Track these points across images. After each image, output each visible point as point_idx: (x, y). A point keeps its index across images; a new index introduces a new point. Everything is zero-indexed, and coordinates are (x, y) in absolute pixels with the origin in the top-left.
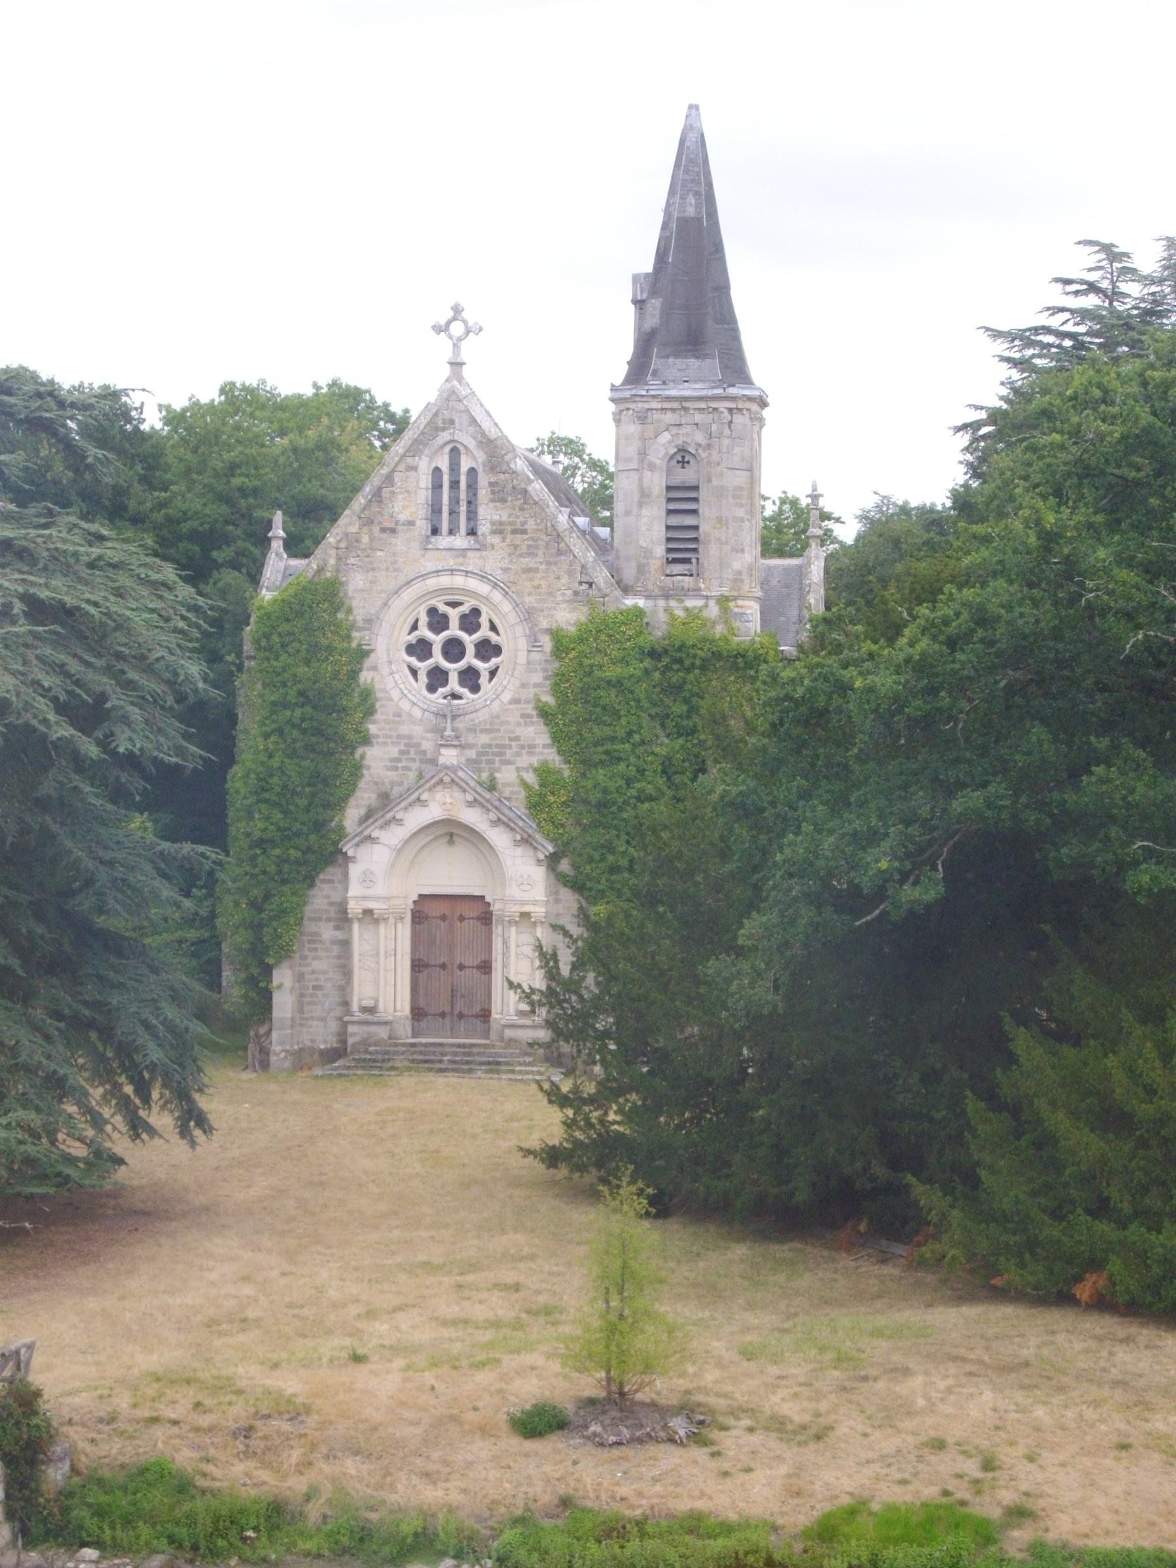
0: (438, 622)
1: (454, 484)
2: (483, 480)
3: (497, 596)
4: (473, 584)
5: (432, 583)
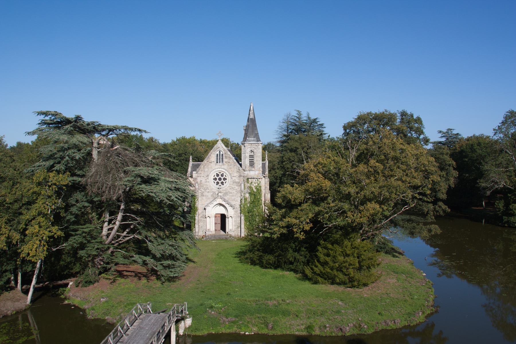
0: (218, 175)
1: (220, 156)
2: (224, 155)
3: (226, 172)
4: (223, 170)
5: (217, 170)
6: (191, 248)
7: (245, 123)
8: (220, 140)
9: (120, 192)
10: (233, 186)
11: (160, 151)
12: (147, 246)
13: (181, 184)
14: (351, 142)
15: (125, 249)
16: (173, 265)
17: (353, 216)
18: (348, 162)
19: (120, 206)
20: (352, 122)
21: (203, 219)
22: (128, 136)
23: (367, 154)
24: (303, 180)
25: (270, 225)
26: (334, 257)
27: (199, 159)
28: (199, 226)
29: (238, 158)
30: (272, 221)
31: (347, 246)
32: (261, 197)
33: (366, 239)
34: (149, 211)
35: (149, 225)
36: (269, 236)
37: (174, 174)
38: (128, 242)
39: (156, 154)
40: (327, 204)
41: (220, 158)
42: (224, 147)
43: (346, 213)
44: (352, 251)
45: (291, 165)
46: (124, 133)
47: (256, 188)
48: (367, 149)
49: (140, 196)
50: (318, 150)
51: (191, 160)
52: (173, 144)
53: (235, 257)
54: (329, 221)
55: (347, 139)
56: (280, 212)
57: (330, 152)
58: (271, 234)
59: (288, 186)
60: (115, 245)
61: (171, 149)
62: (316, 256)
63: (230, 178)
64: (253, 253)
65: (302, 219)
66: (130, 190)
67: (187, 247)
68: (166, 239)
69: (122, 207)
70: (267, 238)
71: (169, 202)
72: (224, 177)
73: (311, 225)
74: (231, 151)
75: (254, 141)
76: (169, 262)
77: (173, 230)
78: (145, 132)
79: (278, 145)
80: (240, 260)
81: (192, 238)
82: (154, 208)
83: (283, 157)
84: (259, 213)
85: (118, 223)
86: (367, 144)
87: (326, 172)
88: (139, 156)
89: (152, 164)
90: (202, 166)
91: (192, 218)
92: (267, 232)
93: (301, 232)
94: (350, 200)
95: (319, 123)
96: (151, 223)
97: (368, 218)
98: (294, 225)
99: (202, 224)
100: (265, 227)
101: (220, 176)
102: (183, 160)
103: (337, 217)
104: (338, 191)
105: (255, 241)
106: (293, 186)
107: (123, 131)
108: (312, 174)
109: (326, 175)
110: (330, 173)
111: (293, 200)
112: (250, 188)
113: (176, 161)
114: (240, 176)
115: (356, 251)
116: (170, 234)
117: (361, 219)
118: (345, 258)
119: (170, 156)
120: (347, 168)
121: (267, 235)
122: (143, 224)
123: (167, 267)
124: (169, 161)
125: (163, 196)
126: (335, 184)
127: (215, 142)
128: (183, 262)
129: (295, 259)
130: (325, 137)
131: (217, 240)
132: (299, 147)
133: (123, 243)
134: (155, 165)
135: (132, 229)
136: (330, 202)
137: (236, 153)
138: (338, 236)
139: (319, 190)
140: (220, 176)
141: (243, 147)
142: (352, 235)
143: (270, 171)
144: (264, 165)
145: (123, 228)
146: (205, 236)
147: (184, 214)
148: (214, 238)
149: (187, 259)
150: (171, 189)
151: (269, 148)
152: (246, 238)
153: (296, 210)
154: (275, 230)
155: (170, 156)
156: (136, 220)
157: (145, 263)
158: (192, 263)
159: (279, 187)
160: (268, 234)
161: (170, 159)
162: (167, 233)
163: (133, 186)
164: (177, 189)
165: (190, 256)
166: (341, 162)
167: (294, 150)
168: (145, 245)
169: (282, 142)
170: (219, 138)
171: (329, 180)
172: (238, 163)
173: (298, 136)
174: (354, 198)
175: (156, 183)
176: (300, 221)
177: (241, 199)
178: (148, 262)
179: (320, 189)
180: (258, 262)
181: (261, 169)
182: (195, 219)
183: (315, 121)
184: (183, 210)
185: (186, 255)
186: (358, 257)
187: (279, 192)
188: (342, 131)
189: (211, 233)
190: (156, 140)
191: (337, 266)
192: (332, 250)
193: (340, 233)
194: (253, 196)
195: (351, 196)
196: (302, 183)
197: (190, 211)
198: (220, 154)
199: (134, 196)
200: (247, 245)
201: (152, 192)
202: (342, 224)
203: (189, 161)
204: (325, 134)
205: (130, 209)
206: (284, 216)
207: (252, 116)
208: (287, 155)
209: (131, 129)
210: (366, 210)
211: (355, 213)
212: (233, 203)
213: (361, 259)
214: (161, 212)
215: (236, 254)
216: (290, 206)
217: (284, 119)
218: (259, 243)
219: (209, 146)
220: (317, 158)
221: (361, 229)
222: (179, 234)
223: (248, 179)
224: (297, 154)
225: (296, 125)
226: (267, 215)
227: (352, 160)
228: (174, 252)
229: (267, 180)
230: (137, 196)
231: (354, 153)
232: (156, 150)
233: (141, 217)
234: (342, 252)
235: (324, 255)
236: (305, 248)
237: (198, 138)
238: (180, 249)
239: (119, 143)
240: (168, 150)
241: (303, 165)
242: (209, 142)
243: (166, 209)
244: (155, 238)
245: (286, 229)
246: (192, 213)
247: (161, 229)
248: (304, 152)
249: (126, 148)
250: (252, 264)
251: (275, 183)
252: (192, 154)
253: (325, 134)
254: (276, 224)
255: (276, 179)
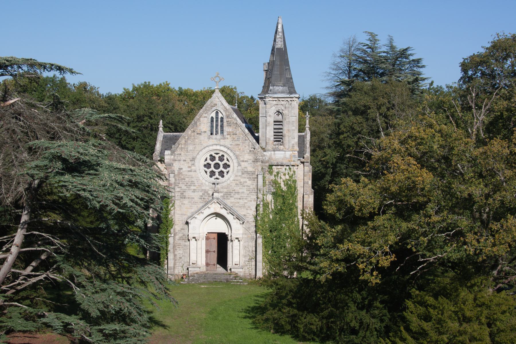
0: (213, 158)
1: (217, 121)
2: (225, 120)
3: (229, 152)
4: (222, 148)
5: (211, 148)
6: (159, 299)
7: (267, 57)
8: (217, 91)
9: (21, 189)
10: (242, 180)
11: (100, 109)
12: (73, 295)
13: (141, 174)
14: (477, 95)
15: (28, 302)
16: (123, 332)
17: (478, 241)
18: (469, 136)
19: (20, 217)
20: (479, 56)
21: (182, 243)
22: (37, 79)
23: (509, 119)
24: (377, 170)
25: (313, 255)
26: (440, 322)
27: (177, 126)
28: (175, 255)
29: (253, 126)
30: (318, 248)
31: (467, 300)
32: (295, 201)
33: (505, 289)
34: (78, 227)
35: (77, 254)
36: (311, 277)
37: (128, 154)
38: (34, 287)
39: (92, 115)
40: (426, 216)
41: (217, 126)
42: (226, 104)
43: (464, 236)
44: (475, 312)
45: (355, 139)
46: (28, 72)
47: (286, 184)
48: (508, 110)
49: (60, 197)
50: (409, 112)
51: (161, 129)
52: (127, 96)
53: (245, 317)
54: (429, 251)
55: (468, 89)
56: (332, 232)
57: (433, 114)
58: (315, 273)
59: (349, 181)
60: (9, 294)
61: (122, 106)
62: (404, 319)
63: (236, 165)
64: (280, 310)
65: (376, 245)
66: (40, 185)
67: (152, 297)
68: (111, 281)
69: (25, 218)
70: (306, 281)
71: (117, 209)
72: (225, 161)
73: (393, 258)
74: (238, 112)
75: (282, 92)
76: (116, 326)
77: (126, 263)
78: (71, 71)
79: (330, 100)
80: (254, 323)
81: (161, 279)
82: (88, 220)
83: (339, 124)
84: (291, 231)
85: (14, 250)
86: (509, 99)
87: (424, 154)
88: (59, 118)
89: (84, 136)
90: (182, 141)
91: (161, 240)
92: (307, 269)
93: (373, 270)
94: (472, 211)
95: (411, 58)
96: (82, 249)
97: (510, 246)
98: (359, 257)
99: (181, 252)
100: (302, 259)
101: (217, 161)
102: (146, 128)
103: (445, 243)
104: (448, 191)
105: (283, 287)
106: (358, 181)
107: (25, 68)
108: (397, 159)
109: (423, 161)
110: (432, 157)
111: (357, 208)
112: (275, 183)
113: (131, 130)
114: (256, 161)
115: (485, 312)
116: (119, 272)
117: (495, 249)
118: (461, 325)
119: (121, 120)
120: (466, 147)
121: (306, 275)
122: (66, 251)
123: (110, 335)
124: (119, 130)
125: (106, 198)
126: (443, 177)
127: (208, 94)
128: (144, 326)
129: (361, 323)
130: (424, 85)
131: (210, 283)
132: (372, 105)
133: (25, 289)
134: (90, 138)
135: (43, 261)
136: (432, 212)
137: (249, 115)
138: (448, 280)
139: (409, 189)
140: (217, 161)
141: (261, 105)
142: (477, 280)
143: (313, 151)
144: (301, 140)
145: (24, 259)
146: (187, 276)
147: (146, 233)
148: (203, 279)
149: (151, 320)
150: (122, 185)
151: (312, 106)
152: (265, 281)
153: (364, 228)
154: (322, 265)
155: (121, 120)
156: (53, 244)
157: (67, 329)
158: (161, 329)
159: (330, 183)
160: (308, 272)
161: (120, 126)
162: (113, 269)
163: (47, 178)
164: (134, 185)
165: (157, 315)
166: (454, 135)
167: (361, 112)
168: (69, 293)
169: (339, 95)
170: (216, 87)
171: (430, 171)
172: (253, 134)
173: (369, 83)
174: (480, 207)
175: (92, 172)
176: (370, 249)
177: (257, 206)
178: (73, 326)
179: (412, 188)
180: (288, 327)
181: (297, 148)
182: (167, 243)
183: (404, 53)
184: (146, 225)
185: (148, 312)
186: (489, 325)
187: (331, 191)
188: (459, 74)
189: (197, 270)
190: (92, 88)
191: (446, 340)
192: (435, 308)
193: (451, 274)
194: (280, 200)
195: (475, 203)
196: (376, 176)
197: (158, 227)
198: (217, 118)
199: (48, 197)
200: (267, 295)
201: (84, 190)
202: (455, 256)
203: (157, 130)
204: (424, 79)
205: (41, 223)
206: (339, 240)
207: (279, 44)
208: (347, 119)
209: (43, 66)
210: (504, 230)
211: (482, 235)
212: (241, 212)
213: (495, 329)
214: (102, 229)
215: (247, 311)
216: (352, 219)
217: (342, 51)
218: (291, 291)
219: (195, 102)
220: (407, 126)
221: (494, 267)
222: (136, 272)
223: (271, 166)
224: (367, 119)
225: (366, 62)
226: (307, 236)
227: (478, 131)
228: (126, 307)
229: (308, 168)
230: (55, 197)
231: (482, 117)
232: (93, 108)
233: (61, 238)
234: (456, 313)
235: (419, 316)
236: (381, 302)
237: (175, 86)
238: (136, 301)
239: (19, 93)
240: (116, 109)
241: (378, 141)
242: (196, 94)
243: (111, 222)
244: (89, 279)
245: (343, 264)
246: (163, 231)
247: (100, 262)
248: (380, 114)
249: (34, 102)
250: (276, 332)
251: (324, 175)
252: (163, 117)
253: (424, 79)
254: (324, 255)
255: (326, 167)
